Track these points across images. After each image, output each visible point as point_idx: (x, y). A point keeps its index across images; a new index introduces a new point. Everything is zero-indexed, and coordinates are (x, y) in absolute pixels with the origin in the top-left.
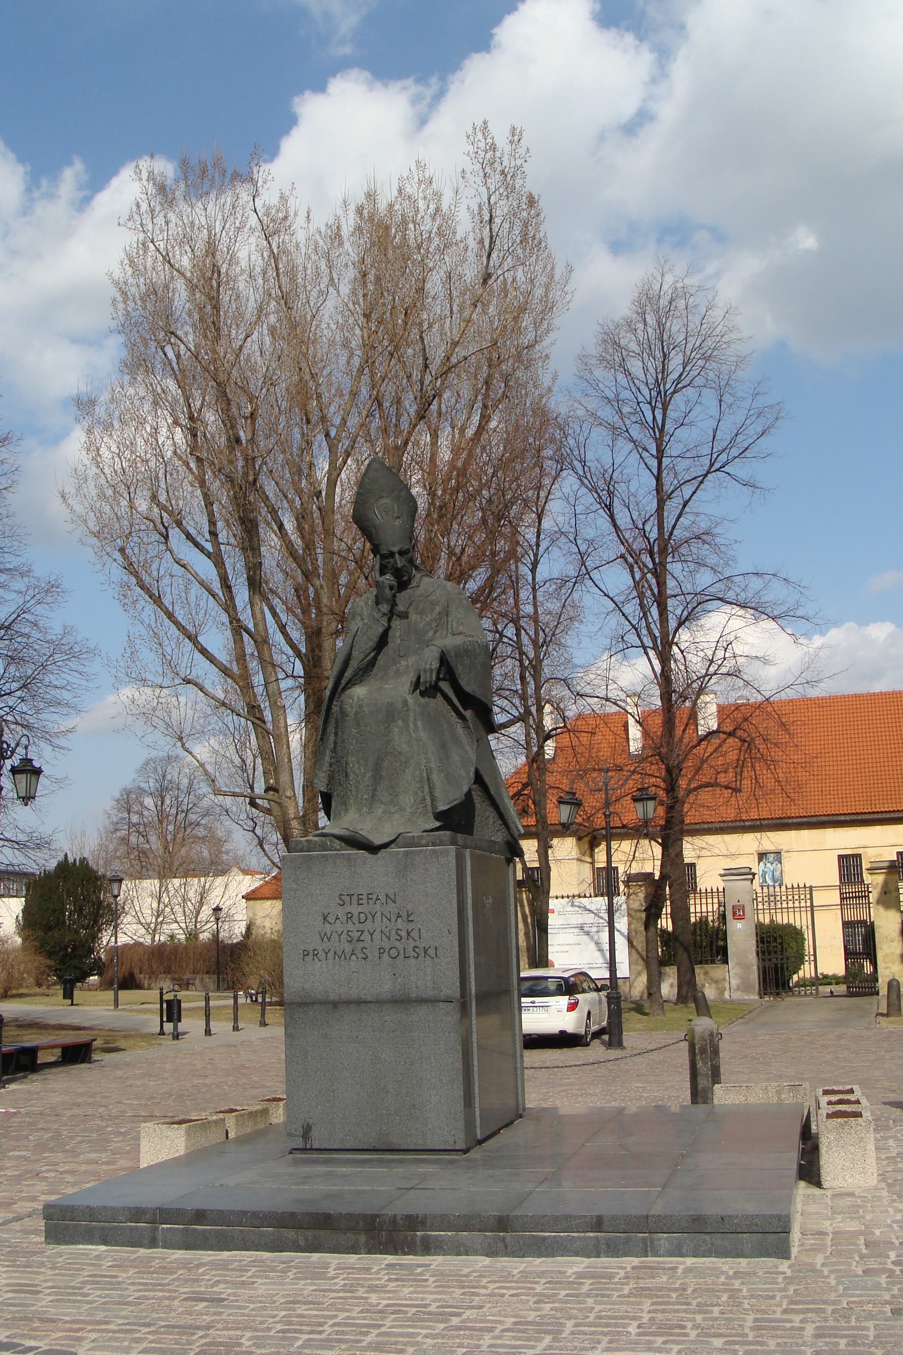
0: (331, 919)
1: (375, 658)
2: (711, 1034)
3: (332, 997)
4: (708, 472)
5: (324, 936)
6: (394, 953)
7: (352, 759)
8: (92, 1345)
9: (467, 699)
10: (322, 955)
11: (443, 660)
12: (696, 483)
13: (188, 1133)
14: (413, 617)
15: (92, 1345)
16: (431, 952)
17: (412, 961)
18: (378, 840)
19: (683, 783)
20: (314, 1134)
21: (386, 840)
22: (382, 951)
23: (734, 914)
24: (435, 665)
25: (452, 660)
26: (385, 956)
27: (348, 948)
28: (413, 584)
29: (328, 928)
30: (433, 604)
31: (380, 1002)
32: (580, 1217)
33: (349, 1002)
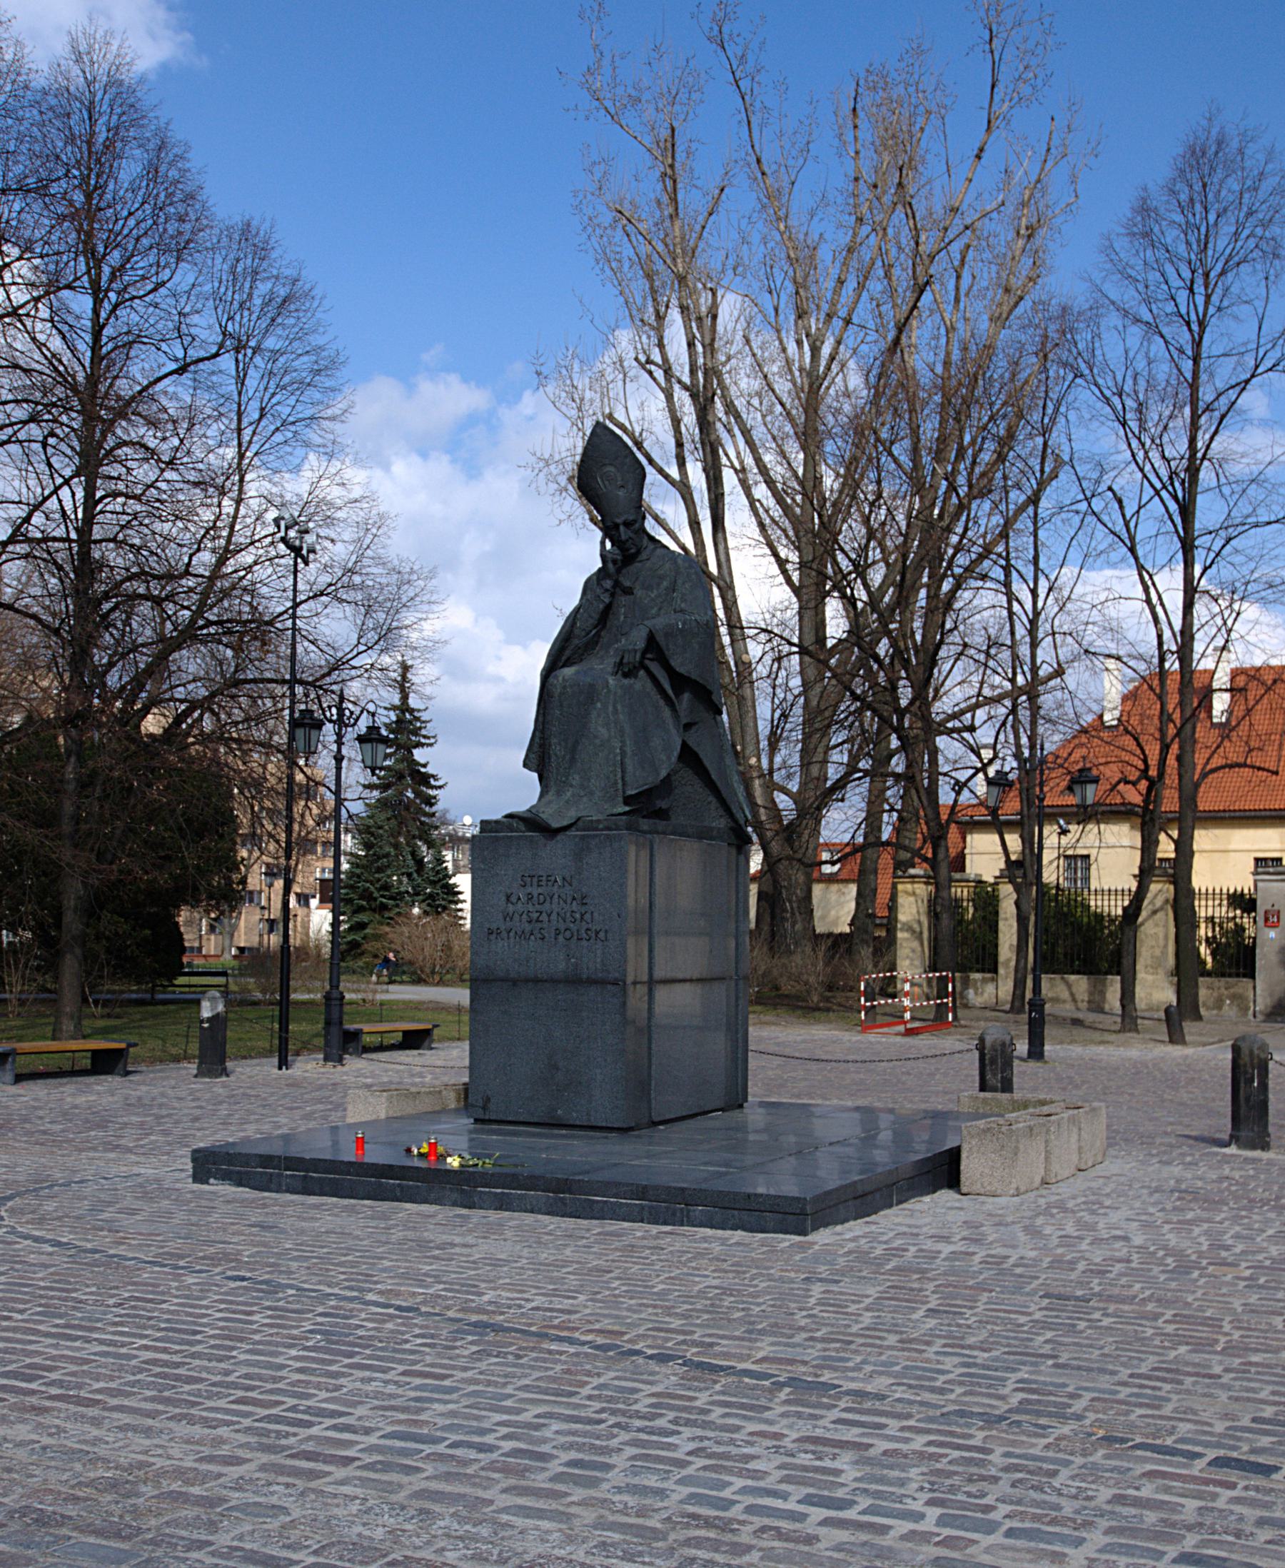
0: (514, 899)
1: (598, 635)
2: (1003, 1044)
3: (513, 975)
4: (1253, 376)
5: (506, 916)
6: (568, 934)
7: (554, 741)
8: (1108, 1539)
9: (681, 682)
10: (504, 934)
11: (651, 639)
12: (1238, 389)
13: (389, 1099)
14: (639, 592)
15: (1108, 1539)
16: (602, 935)
17: (584, 943)
18: (555, 824)
19: (1200, 758)
20: (492, 1106)
21: (565, 823)
22: (558, 932)
23: (1266, 920)
24: (641, 645)
25: (660, 639)
26: (561, 938)
27: (528, 927)
28: (644, 556)
29: (511, 908)
30: (662, 578)
31: (554, 981)
32: (627, 1185)
33: (527, 981)
